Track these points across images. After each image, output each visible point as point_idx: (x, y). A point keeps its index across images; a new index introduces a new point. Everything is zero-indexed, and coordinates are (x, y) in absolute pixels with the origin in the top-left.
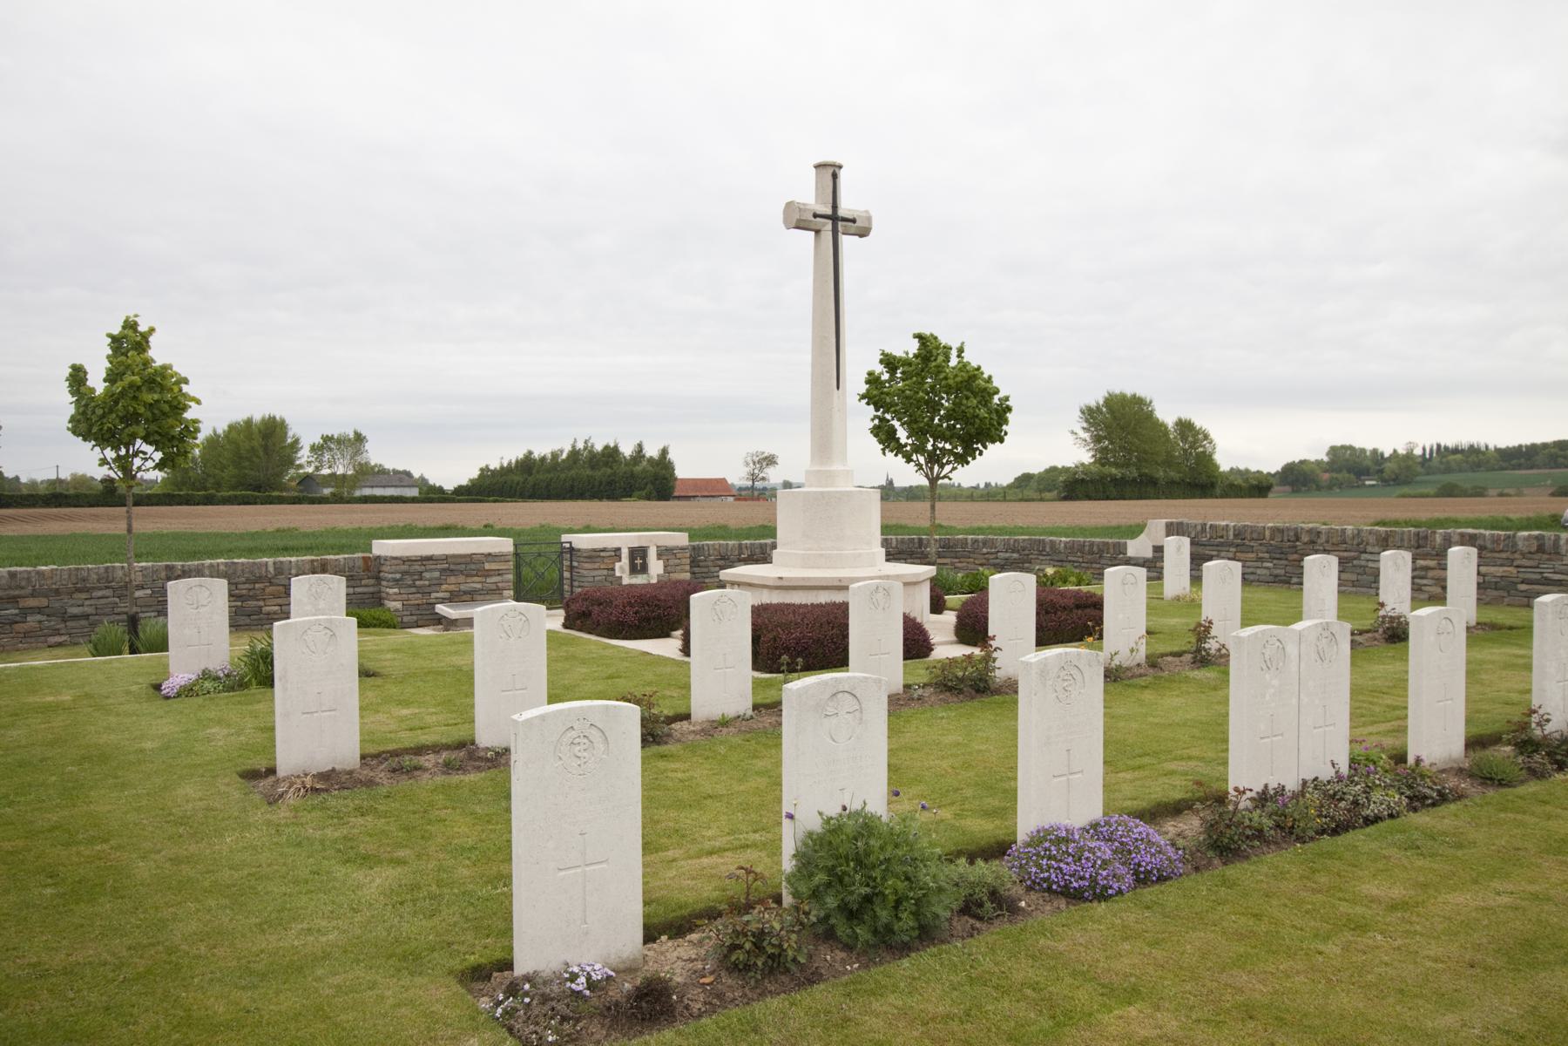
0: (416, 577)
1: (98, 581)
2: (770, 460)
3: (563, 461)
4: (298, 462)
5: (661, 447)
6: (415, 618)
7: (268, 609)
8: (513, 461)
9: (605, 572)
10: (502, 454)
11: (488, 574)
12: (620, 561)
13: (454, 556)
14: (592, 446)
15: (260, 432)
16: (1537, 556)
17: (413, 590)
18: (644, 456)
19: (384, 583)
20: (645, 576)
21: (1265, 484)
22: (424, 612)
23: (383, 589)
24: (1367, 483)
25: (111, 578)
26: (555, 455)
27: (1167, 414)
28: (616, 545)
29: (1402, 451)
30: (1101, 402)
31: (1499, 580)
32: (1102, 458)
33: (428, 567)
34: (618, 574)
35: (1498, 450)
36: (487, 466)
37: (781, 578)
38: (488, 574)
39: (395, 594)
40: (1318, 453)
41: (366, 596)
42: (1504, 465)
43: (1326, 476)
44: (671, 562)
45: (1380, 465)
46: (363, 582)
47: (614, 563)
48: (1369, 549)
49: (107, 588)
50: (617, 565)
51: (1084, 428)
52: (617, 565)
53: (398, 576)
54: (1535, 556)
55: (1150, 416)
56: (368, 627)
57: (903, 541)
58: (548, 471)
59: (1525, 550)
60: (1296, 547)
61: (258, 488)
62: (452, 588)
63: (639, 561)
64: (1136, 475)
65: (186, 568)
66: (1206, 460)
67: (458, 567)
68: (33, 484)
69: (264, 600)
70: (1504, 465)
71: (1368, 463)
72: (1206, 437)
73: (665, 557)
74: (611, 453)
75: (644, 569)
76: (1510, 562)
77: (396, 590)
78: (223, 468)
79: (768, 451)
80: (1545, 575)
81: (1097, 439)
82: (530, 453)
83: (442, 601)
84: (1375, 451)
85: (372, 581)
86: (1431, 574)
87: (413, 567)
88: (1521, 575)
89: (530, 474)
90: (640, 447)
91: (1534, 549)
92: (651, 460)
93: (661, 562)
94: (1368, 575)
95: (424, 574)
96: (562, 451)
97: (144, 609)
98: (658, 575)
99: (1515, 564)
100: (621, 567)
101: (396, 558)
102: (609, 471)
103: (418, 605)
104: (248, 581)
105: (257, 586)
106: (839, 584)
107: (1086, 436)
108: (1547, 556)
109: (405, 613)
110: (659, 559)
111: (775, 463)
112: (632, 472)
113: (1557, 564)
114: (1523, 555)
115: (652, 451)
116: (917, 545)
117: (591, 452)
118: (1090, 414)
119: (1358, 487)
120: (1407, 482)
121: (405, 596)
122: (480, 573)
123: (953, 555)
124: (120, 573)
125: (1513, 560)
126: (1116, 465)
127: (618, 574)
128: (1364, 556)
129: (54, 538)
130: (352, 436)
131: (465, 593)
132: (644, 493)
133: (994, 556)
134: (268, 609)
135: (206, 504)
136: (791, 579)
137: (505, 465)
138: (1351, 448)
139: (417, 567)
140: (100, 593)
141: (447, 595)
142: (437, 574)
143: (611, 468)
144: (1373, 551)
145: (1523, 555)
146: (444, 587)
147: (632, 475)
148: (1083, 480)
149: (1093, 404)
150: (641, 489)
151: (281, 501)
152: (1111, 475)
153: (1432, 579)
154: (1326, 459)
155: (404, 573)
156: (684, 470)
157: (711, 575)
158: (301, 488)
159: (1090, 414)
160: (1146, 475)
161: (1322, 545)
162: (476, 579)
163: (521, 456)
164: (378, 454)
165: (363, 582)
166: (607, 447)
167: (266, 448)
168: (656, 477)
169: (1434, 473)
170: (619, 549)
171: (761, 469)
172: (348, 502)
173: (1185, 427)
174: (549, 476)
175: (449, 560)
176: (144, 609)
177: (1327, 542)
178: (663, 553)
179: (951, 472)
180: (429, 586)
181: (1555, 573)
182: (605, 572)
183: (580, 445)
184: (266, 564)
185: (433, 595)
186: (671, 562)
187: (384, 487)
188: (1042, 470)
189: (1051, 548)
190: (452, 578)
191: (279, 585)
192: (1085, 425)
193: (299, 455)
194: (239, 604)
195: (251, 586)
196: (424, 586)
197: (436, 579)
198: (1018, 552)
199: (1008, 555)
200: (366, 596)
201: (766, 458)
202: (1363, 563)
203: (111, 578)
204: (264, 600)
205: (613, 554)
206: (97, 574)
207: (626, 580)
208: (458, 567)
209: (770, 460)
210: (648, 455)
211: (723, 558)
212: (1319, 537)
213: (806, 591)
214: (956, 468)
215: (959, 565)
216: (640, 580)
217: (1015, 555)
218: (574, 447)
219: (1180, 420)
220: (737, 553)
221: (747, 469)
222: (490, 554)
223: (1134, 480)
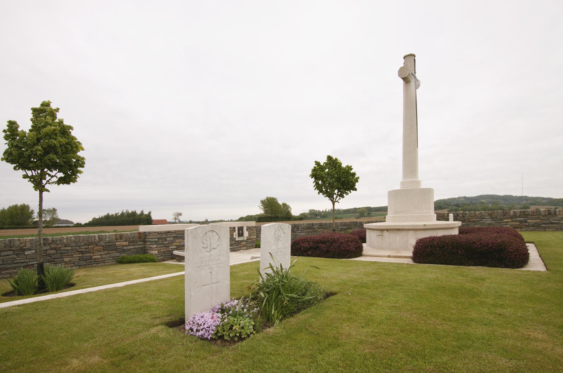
0: (164, 240)
1: (5, 247)
2: (180, 214)
3: (119, 216)
4: (33, 217)
5: (149, 211)
6: (163, 257)
7: (95, 257)
8: (103, 216)
10: (100, 214)
13: (178, 231)
14: (128, 212)
15: (20, 208)
16: (548, 216)
17: (162, 245)
18: (143, 214)
19: (147, 243)
21: (302, 217)
22: (166, 255)
23: (147, 246)
24: (318, 217)
25: (12, 246)
26: (116, 214)
27: (280, 202)
29: (324, 210)
30: (265, 199)
31: (534, 224)
32: (266, 212)
34: (234, 237)
35: (343, 210)
36: (95, 218)
37: (425, 225)
39: (155, 247)
40: (307, 211)
41: (140, 249)
42: (344, 213)
43: (309, 216)
44: (251, 232)
45: (320, 213)
46: (138, 243)
47: (233, 233)
48: (485, 217)
49: (10, 250)
50: (234, 233)
51: (262, 205)
52: (234, 233)
53: (156, 240)
54: (547, 216)
55: (277, 202)
56: (144, 262)
58: (115, 218)
59: (544, 214)
60: (457, 218)
61: (19, 225)
62: (177, 244)
63: (241, 232)
64: (274, 216)
65: (54, 239)
66: (289, 213)
67: (180, 235)
69: (93, 253)
70: (344, 213)
71: (318, 213)
72: (289, 207)
73: (249, 230)
74: (134, 213)
76: (538, 218)
77: (156, 246)
78: (6, 220)
79: (180, 212)
80: (551, 221)
81: (265, 208)
82: (109, 214)
83: (174, 249)
84: (319, 210)
85: (142, 243)
86: (509, 223)
87: (162, 236)
88: (542, 222)
89: (108, 219)
90: (142, 211)
91: (547, 214)
92: (146, 215)
93: (248, 232)
94: (485, 225)
95: (167, 239)
96: (119, 213)
97: (30, 260)
98: (247, 237)
99: (540, 219)
100: (236, 234)
101: (155, 232)
102: (133, 218)
103: (164, 252)
104: (85, 244)
105: (90, 247)
106: (424, 227)
107: (262, 207)
108: (551, 216)
109: (159, 255)
110: (247, 231)
111: (182, 215)
112: (140, 218)
113: (556, 218)
114: (543, 216)
115: (146, 213)
116: (311, 226)
117: (128, 213)
118: (263, 202)
119: (316, 218)
120: (326, 217)
121: (159, 248)
124: (18, 243)
125: (539, 218)
126: (270, 214)
127: (234, 237)
128: (483, 220)
130: (52, 209)
132: (144, 223)
133: (337, 228)
134: (95, 257)
136: (429, 225)
137: (101, 217)
138: (314, 210)
140: (5, 253)
141: (175, 247)
142: (172, 239)
143: (134, 217)
144: (487, 218)
145: (543, 216)
146: (174, 244)
147: (140, 219)
148: (262, 217)
149: (263, 200)
150: (143, 222)
151: (27, 228)
152: (268, 216)
153: (509, 225)
154: (309, 212)
155: (159, 238)
156: (154, 217)
158: (34, 225)
159: (263, 202)
160: (276, 216)
161: (467, 217)
163: (105, 215)
164: (61, 216)
165: (138, 243)
166: (132, 212)
167: (22, 213)
168: (147, 219)
169: (331, 215)
170: (235, 228)
171: (178, 217)
172: (51, 228)
173: (284, 205)
174: (115, 220)
175: (177, 233)
176: (30, 260)
177: (469, 216)
178: (249, 229)
179: (339, 200)
180: (169, 243)
181: (555, 220)
183: (125, 211)
184: (95, 237)
185: (170, 247)
187: (62, 224)
188: (245, 216)
189: (360, 224)
190: (178, 240)
191: (101, 246)
192: (262, 205)
193: (33, 215)
194: (81, 255)
195: (87, 247)
196: (167, 244)
197: (172, 240)
198: (346, 226)
199: (342, 227)
200: (140, 249)
201: (179, 214)
202: (484, 222)
203: (12, 246)
204: (93, 253)
206: (5, 243)
207: (237, 239)
208: (180, 235)
209: (180, 214)
210: (145, 214)
212: (466, 215)
213: (433, 231)
214: (340, 199)
215: (325, 231)
216: (241, 239)
217: (345, 227)
218: (122, 212)
219: (283, 203)
221: (174, 217)
223: (274, 217)
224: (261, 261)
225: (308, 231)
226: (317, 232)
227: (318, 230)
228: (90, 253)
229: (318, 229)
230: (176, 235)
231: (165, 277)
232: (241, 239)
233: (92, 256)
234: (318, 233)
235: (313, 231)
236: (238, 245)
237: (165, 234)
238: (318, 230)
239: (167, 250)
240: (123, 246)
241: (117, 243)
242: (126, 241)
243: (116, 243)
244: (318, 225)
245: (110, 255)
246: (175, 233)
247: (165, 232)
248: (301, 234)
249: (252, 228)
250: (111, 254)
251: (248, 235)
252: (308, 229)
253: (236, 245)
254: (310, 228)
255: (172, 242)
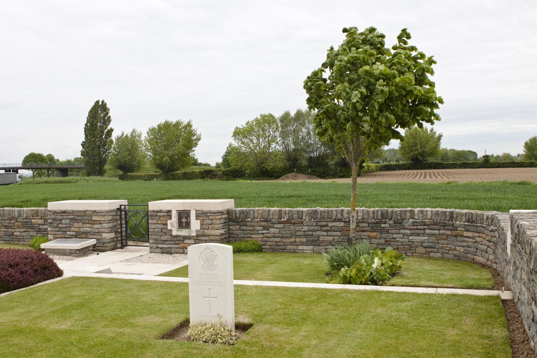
0: (58, 222)
9: (161, 226)
11: (94, 222)
12: (171, 219)
13: (76, 211)
17: (57, 229)
20: (187, 230)
28: (168, 208)
33: (64, 217)
34: (169, 228)
38: (94, 222)
44: (206, 222)
47: (167, 220)
50: (169, 222)
52: (169, 222)
57: (437, 213)
62: (76, 229)
68: (498, 157)
73: (200, 218)
75: (188, 225)
87: (58, 217)
93: (199, 221)
98: (196, 230)
100: (171, 223)
110: (197, 219)
122: (90, 222)
123: (474, 229)
127: (169, 228)
129: (369, 185)
131: (83, 233)
135: (530, 167)
139: (59, 217)
141: (74, 233)
146: (72, 229)
155: (54, 219)
157: (256, 232)
162: (88, 225)
170: (170, 211)
178: (201, 215)
182: (161, 226)
186: (206, 222)
190: (76, 224)
194: (5, 230)
195: (9, 222)
197: (68, 224)
205: (166, 214)
207: (175, 233)
211: (266, 221)
216: (184, 232)
220: (277, 217)
222: (95, 211)
224: (233, 279)
225: (436, 232)
226: (462, 239)
227: (466, 234)
228: (12, 229)
229: (467, 231)
230: (73, 216)
231: (174, 269)
232: (184, 232)
233: (13, 232)
234: (464, 241)
235: (451, 235)
236: (178, 244)
237: (60, 214)
238: (466, 234)
239: (63, 236)
240: (39, 225)
241: (33, 221)
242: (41, 219)
243: (33, 220)
244: (464, 220)
245: (27, 233)
246: (72, 214)
247: (60, 212)
248: (411, 238)
249: (208, 215)
250: (30, 232)
251: (198, 227)
252: (438, 227)
253: (172, 242)
254: (444, 226)
255: (69, 226)
